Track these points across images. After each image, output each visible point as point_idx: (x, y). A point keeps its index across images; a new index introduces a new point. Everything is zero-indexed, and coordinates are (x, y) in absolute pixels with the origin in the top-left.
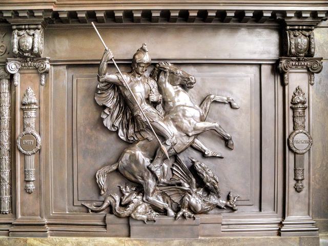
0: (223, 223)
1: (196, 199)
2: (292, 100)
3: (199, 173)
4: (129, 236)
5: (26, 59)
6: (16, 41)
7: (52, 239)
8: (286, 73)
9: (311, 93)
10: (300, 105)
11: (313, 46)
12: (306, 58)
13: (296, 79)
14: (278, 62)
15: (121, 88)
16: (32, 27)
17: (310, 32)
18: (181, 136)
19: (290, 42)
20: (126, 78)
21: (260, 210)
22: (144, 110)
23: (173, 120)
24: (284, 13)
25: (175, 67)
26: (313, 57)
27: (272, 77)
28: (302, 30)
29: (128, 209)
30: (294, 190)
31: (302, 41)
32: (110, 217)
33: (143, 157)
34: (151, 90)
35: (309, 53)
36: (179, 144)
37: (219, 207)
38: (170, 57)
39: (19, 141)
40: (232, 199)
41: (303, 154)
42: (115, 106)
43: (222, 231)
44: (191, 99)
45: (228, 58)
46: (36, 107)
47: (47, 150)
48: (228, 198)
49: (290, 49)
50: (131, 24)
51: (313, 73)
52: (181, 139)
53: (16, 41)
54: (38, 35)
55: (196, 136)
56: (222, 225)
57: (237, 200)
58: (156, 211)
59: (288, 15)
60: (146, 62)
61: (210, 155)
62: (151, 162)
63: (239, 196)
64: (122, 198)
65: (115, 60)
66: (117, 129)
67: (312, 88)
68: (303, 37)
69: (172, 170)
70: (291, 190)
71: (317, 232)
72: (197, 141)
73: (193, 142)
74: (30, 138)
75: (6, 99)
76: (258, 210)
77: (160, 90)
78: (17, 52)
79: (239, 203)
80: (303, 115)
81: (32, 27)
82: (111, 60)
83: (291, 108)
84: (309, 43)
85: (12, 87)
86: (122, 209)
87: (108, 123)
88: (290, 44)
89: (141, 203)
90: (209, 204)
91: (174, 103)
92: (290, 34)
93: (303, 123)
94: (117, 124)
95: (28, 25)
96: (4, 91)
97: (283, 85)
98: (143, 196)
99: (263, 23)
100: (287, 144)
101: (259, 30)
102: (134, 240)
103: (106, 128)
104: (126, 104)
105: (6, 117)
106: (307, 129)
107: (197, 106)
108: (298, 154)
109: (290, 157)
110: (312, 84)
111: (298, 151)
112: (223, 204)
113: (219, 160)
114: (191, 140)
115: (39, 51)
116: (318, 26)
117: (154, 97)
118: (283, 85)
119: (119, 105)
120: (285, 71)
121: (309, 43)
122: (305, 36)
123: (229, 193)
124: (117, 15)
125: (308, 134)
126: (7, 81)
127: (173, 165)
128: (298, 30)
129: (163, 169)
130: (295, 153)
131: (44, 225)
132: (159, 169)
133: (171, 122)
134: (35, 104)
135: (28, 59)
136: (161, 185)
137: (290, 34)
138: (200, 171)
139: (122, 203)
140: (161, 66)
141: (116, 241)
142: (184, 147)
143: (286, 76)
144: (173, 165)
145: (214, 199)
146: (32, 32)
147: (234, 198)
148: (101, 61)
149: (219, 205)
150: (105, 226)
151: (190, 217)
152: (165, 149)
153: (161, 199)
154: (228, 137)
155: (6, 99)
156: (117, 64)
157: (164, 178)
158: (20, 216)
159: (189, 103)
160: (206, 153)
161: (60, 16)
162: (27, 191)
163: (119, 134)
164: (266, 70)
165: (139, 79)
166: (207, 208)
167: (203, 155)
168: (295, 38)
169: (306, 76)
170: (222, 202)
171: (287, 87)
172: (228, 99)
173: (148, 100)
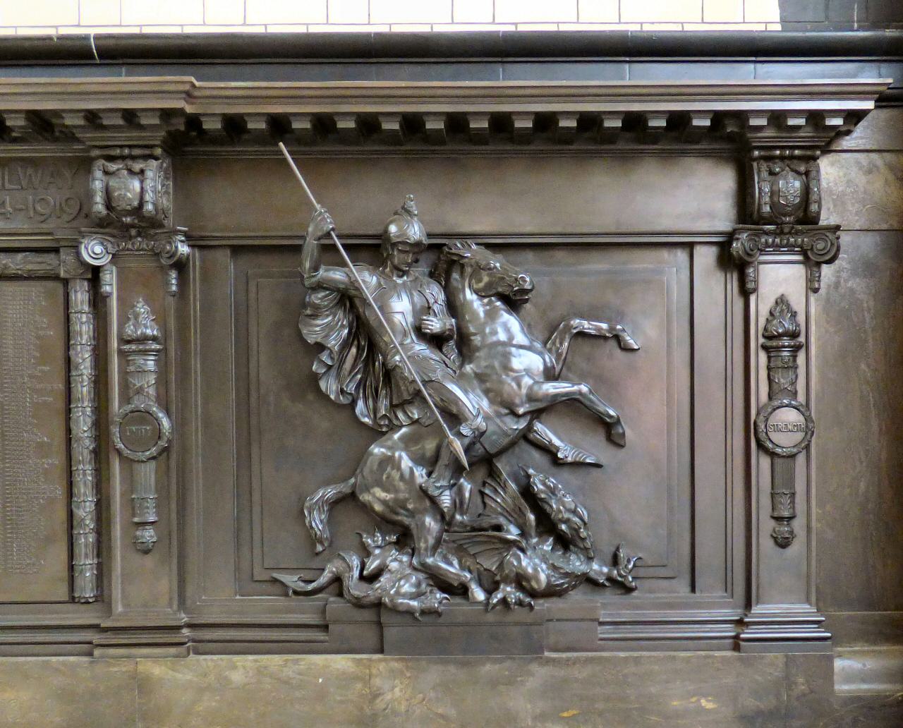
0: (601, 620)
1: (537, 562)
2: (765, 329)
3: (542, 500)
4: (381, 651)
5: (127, 230)
6: (98, 185)
7: (198, 661)
8: (752, 263)
9: (813, 310)
10: (786, 341)
11: (814, 197)
12: (800, 227)
13: (780, 277)
14: (731, 236)
15: (357, 302)
16: (136, 152)
17: (812, 162)
18: (499, 415)
19: (760, 189)
20: (367, 280)
21: (693, 589)
22: (409, 356)
23: (481, 378)
24: (741, 116)
25: (488, 253)
26: (817, 224)
27: (720, 276)
28: (792, 157)
29: (378, 585)
30: (771, 543)
31: (791, 186)
32: (335, 604)
33: (410, 464)
34: (429, 308)
35: (805, 215)
36: (494, 433)
37: (589, 581)
38: (477, 228)
39: (115, 430)
40: (623, 562)
41: (793, 456)
42: (346, 345)
43: (601, 639)
44: (528, 328)
45: (613, 230)
46: (158, 347)
47: (185, 450)
48: (615, 561)
49: (759, 205)
50: (425, 148)
51: (818, 264)
52: (498, 421)
53: (98, 185)
54: (153, 171)
55: (536, 414)
56: (602, 624)
57: (634, 566)
58: (443, 590)
59: (754, 122)
60: (411, 241)
61: (570, 459)
62: (429, 474)
63: (640, 555)
64: (366, 560)
65: (339, 237)
66: (350, 398)
67: (817, 300)
68: (791, 175)
69: (482, 494)
70: (764, 545)
71: (829, 643)
72: (538, 426)
73: (529, 428)
74: (142, 421)
75: (84, 328)
76: (688, 589)
77: (453, 307)
78: (104, 212)
79: (642, 572)
80: (791, 364)
81: (136, 152)
82: (328, 235)
83: (764, 348)
84: (806, 192)
85: (98, 302)
86: (364, 585)
87: (329, 386)
88: (760, 193)
89: (408, 571)
90: (567, 575)
91: (484, 336)
92: (759, 171)
93: (793, 383)
94: (351, 388)
95: (130, 147)
96: (80, 308)
97: (745, 293)
98: (412, 555)
99: (697, 143)
100: (755, 438)
101: (689, 161)
102: (392, 659)
103: (327, 397)
104: (365, 335)
105: (85, 372)
106: (801, 398)
107: (538, 345)
108: (778, 455)
109: (763, 464)
110: (816, 291)
111: (778, 450)
112: (602, 573)
113: (595, 471)
114: (522, 425)
115: (156, 209)
116: (834, 148)
117: (435, 325)
118: (745, 293)
119: (356, 343)
120: (175, 259)
121: (806, 192)
122: (798, 173)
123: (618, 549)
124: (341, 125)
125: (804, 409)
126: (86, 283)
127: (484, 484)
128: (782, 158)
129: (460, 491)
130: (772, 455)
131: (179, 628)
132: (447, 492)
133: (475, 382)
134: (154, 339)
135: (133, 232)
136: (456, 529)
137: (759, 171)
138: (543, 496)
139: (365, 573)
140: (453, 251)
141: (350, 664)
142: (506, 441)
143: (751, 270)
144: (484, 484)
145: (578, 564)
146: (137, 166)
147: (629, 561)
148: (303, 238)
149: (592, 575)
150: (325, 628)
151: (520, 603)
152: (458, 446)
153: (455, 562)
154: (611, 417)
155: (84, 328)
156: (343, 245)
157: (462, 514)
158: (119, 608)
159: (520, 338)
160: (560, 455)
161: (472, 126)
162: (158, 616)
163: (358, 411)
164: (706, 257)
165: (399, 281)
166: (563, 584)
167: (556, 462)
168: (770, 178)
169: (800, 270)
170: (598, 569)
171: (753, 298)
172: (611, 329)
173: (419, 331)
